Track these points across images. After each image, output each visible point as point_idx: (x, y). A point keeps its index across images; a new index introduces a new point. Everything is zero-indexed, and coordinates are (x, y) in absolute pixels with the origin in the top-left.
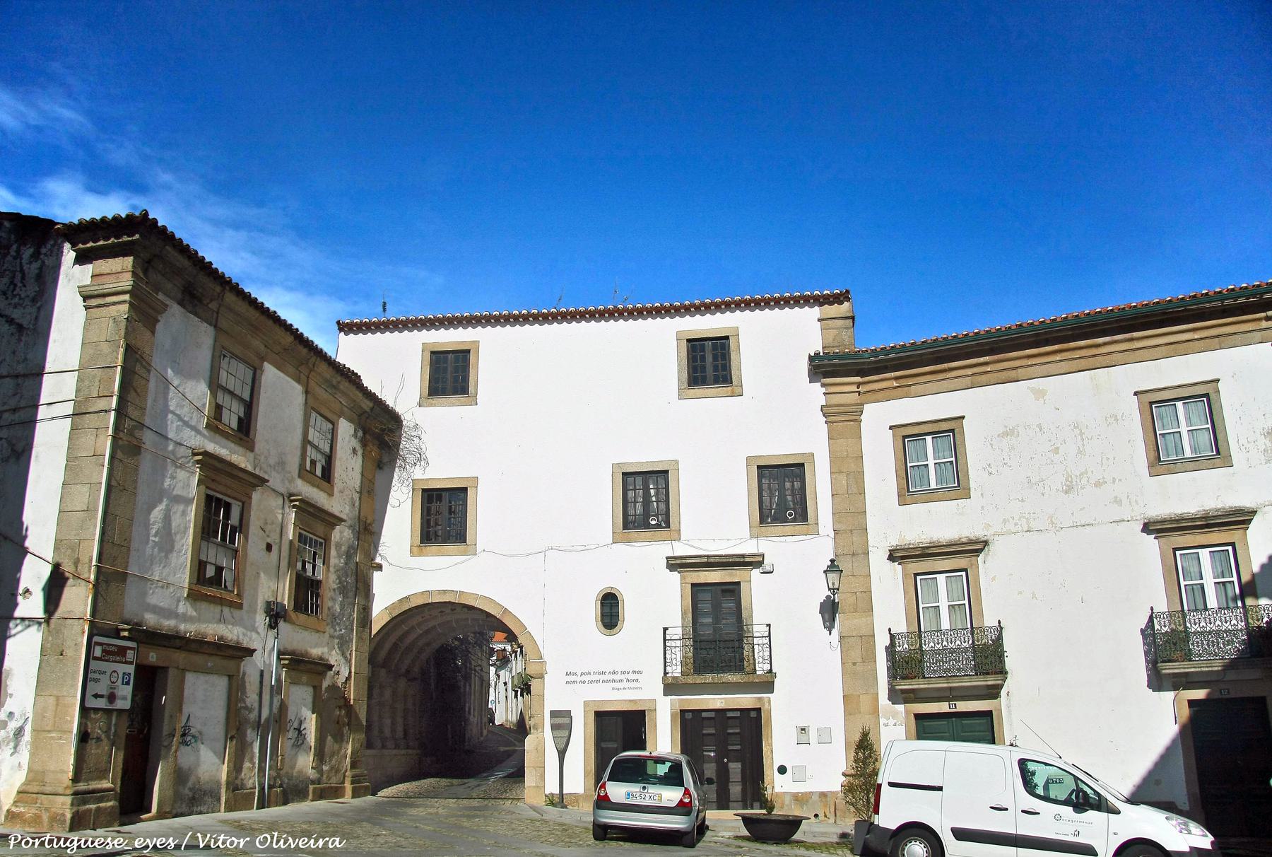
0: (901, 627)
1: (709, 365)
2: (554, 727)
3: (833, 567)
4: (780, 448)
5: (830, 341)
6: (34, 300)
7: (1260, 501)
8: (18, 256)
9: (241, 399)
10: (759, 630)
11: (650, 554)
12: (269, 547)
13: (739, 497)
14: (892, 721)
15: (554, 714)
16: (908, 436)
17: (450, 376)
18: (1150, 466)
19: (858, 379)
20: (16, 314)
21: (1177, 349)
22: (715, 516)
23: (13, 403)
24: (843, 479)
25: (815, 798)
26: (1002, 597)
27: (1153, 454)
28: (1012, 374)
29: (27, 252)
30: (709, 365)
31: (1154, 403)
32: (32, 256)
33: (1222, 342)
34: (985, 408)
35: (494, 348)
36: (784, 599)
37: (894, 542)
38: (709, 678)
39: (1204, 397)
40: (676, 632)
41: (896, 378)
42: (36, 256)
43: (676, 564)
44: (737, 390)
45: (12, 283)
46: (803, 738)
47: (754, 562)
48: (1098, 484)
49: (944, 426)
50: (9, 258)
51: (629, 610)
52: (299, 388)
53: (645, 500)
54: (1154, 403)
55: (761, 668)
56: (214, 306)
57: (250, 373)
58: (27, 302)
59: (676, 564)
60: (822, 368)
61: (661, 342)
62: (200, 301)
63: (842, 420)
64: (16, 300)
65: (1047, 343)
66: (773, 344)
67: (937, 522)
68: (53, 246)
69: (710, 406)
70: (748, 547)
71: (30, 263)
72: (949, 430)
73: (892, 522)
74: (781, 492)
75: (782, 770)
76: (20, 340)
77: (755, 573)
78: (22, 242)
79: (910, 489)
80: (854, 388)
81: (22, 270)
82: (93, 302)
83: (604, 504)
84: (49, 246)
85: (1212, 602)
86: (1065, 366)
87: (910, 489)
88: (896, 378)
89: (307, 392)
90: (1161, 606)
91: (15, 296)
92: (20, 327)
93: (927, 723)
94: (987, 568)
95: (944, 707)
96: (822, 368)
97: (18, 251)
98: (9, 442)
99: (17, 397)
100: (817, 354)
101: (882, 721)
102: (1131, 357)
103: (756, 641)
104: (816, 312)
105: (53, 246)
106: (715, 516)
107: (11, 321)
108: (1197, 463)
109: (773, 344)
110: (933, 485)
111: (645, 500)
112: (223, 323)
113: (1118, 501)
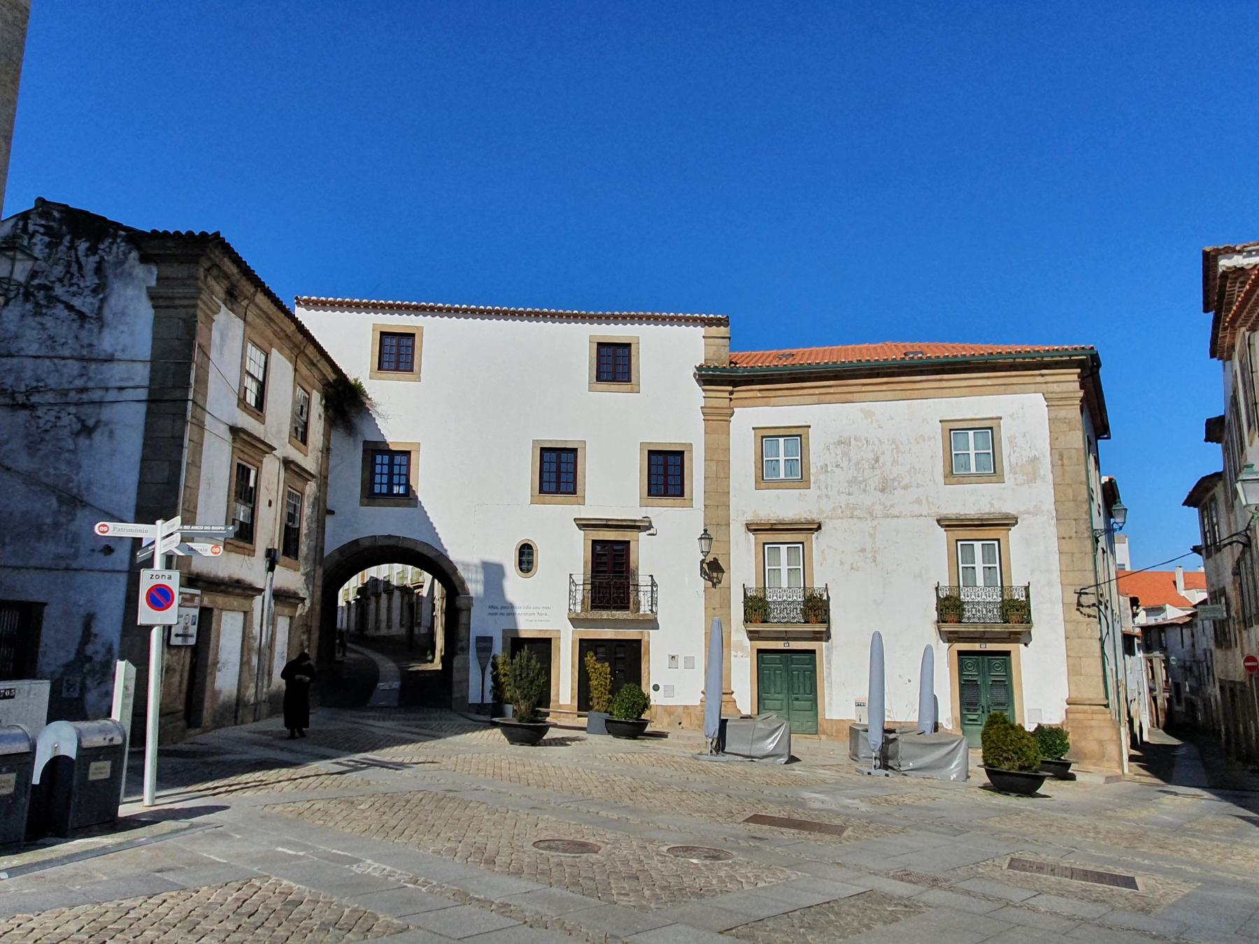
0: (752, 584)
1: (614, 364)
2: (479, 650)
3: (706, 536)
4: (666, 439)
5: (710, 356)
6: (95, 291)
7: (1022, 509)
8: (72, 247)
9: (257, 380)
10: (643, 580)
11: (561, 512)
12: (270, 503)
13: (635, 474)
14: (740, 654)
15: (480, 639)
16: (766, 436)
17: (397, 353)
18: (945, 477)
19: (730, 388)
20: (77, 302)
21: (973, 391)
22: (613, 487)
23: (79, 383)
24: (713, 465)
25: (680, 710)
26: (829, 567)
27: (948, 469)
28: (849, 397)
29: (83, 246)
30: (614, 364)
31: (954, 431)
32: (88, 249)
33: (1006, 389)
34: (824, 417)
35: (434, 333)
36: (666, 556)
37: (750, 517)
38: (605, 614)
39: (988, 429)
40: (579, 579)
41: (760, 390)
42: (92, 250)
43: (584, 525)
44: (636, 388)
45: (68, 272)
46: (674, 662)
47: (634, 526)
48: (905, 488)
49: (794, 432)
50: (61, 248)
51: (541, 558)
52: (291, 367)
53: (558, 470)
54: (954, 431)
55: (645, 608)
56: (244, 303)
57: (263, 357)
58: (87, 292)
59: (584, 525)
60: (708, 377)
61: (577, 341)
62: (236, 299)
63: (717, 419)
64: (75, 288)
65: (878, 376)
66: (672, 352)
67: (784, 505)
68: (112, 243)
69: (613, 397)
70: (634, 512)
71: (87, 256)
72: (797, 435)
73: (751, 501)
74: (665, 473)
75: (656, 688)
76: (82, 327)
77: (643, 535)
78: (76, 236)
79: (764, 477)
80: (727, 395)
81: (78, 262)
82: (162, 303)
83: (527, 471)
84: (107, 244)
85: (980, 582)
86: (890, 395)
87: (764, 477)
88: (760, 390)
89: (296, 370)
90: (945, 583)
91: (71, 285)
92: (82, 316)
93: (766, 656)
94: (818, 543)
95: (780, 645)
96: (708, 377)
97: (72, 242)
98: (79, 419)
99: (85, 378)
100: (701, 366)
101: (733, 653)
102: (939, 392)
103: (641, 589)
104: (700, 331)
105: (112, 243)
106: (613, 487)
107: (70, 308)
108: (979, 478)
109: (672, 352)
110: (782, 476)
111: (558, 470)
112: (250, 317)
113: (918, 501)
